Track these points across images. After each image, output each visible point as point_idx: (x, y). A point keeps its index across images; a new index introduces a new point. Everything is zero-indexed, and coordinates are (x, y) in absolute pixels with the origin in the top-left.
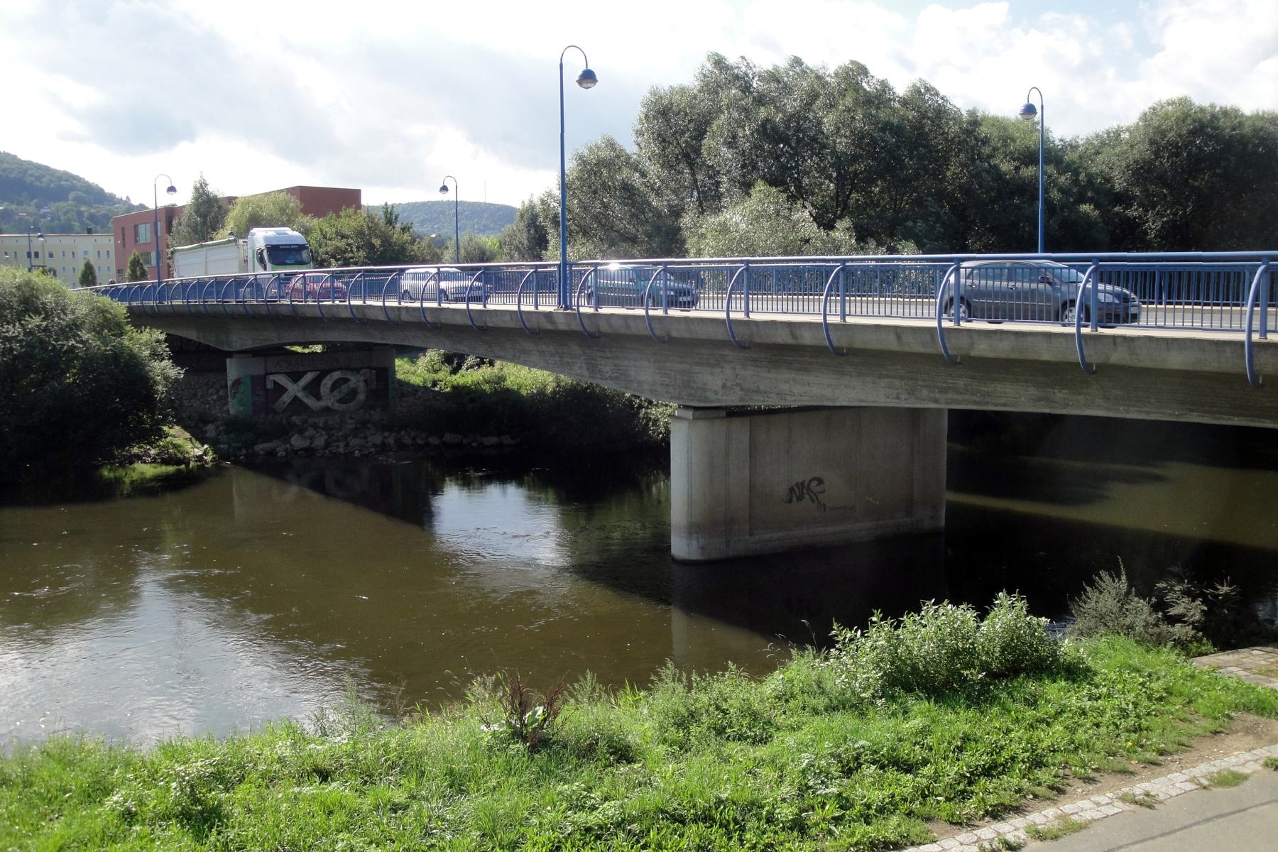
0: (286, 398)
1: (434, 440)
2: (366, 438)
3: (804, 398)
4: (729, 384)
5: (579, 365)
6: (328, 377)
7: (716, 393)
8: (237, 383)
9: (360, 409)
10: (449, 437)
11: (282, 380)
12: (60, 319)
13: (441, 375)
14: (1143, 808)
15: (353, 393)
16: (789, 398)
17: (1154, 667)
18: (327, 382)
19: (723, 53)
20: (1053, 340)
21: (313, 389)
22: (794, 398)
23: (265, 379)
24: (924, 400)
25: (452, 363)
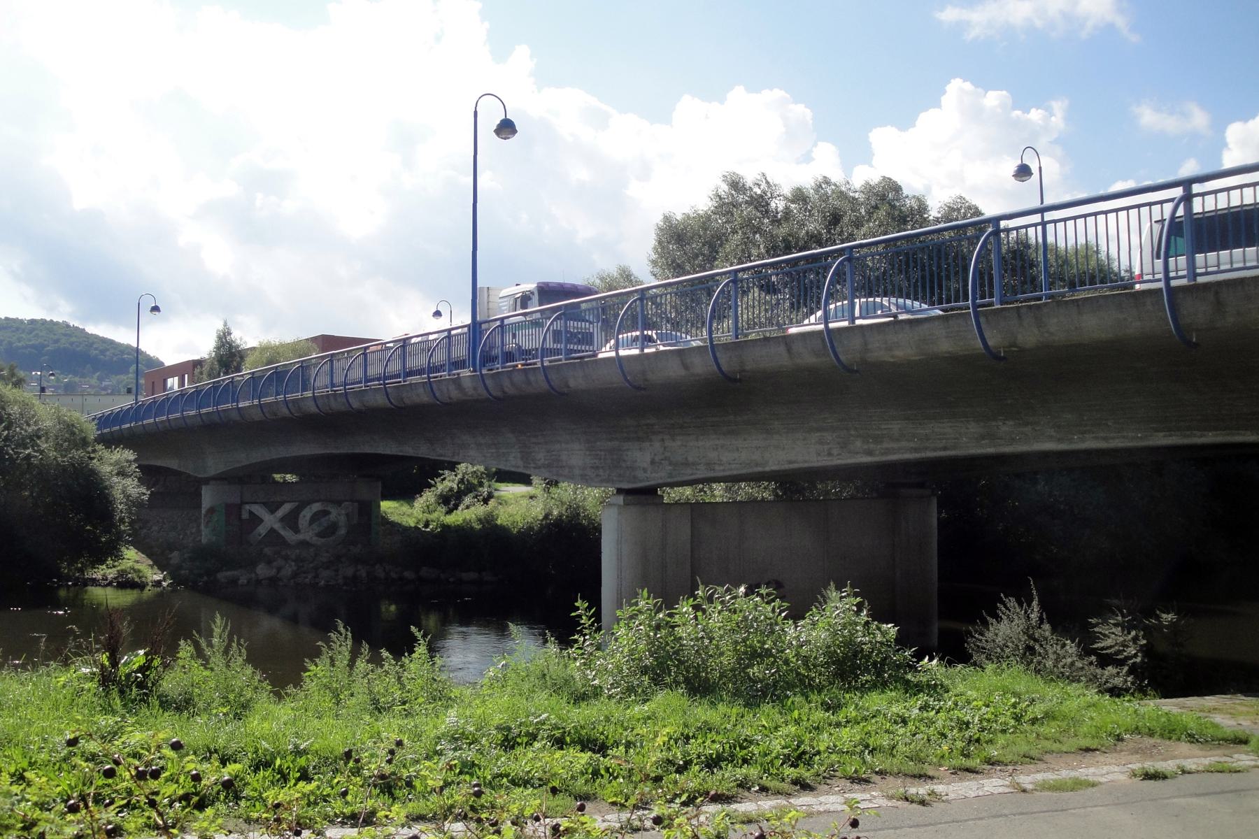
0: (262, 530)
1: (408, 574)
2: (337, 571)
3: (733, 466)
4: (657, 459)
5: (513, 455)
7: (645, 470)
8: (211, 511)
9: (339, 544)
10: (425, 572)
11: (259, 510)
12: (22, 429)
13: (434, 516)
14: (914, 805)
16: (717, 468)
18: (307, 514)
19: (740, 172)
20: (950, 322)
21: (291, 521)
22: (722, 468)
23: (240, 508)
24: (857, 453)
25: (449, 504)
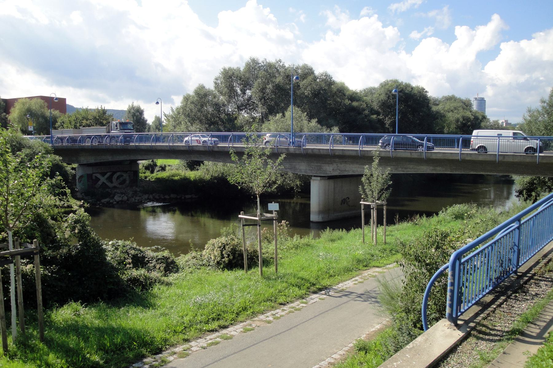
0: (100, 183)
4: (335, 169)
6: (115, 175)
11: (99, 176)
18: (115, 176)
21: (110, 179)
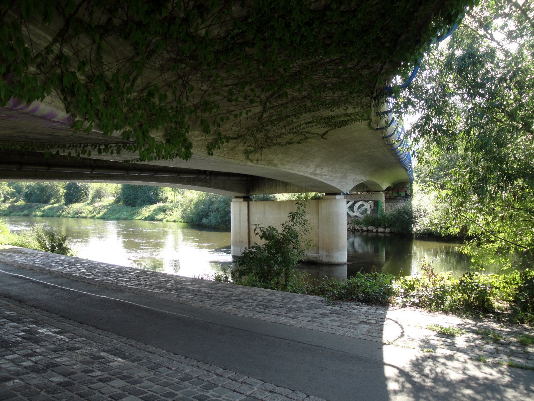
10: (370, 228)
15: (366, 210)
17: (201, 140)
18: (357, 206)
